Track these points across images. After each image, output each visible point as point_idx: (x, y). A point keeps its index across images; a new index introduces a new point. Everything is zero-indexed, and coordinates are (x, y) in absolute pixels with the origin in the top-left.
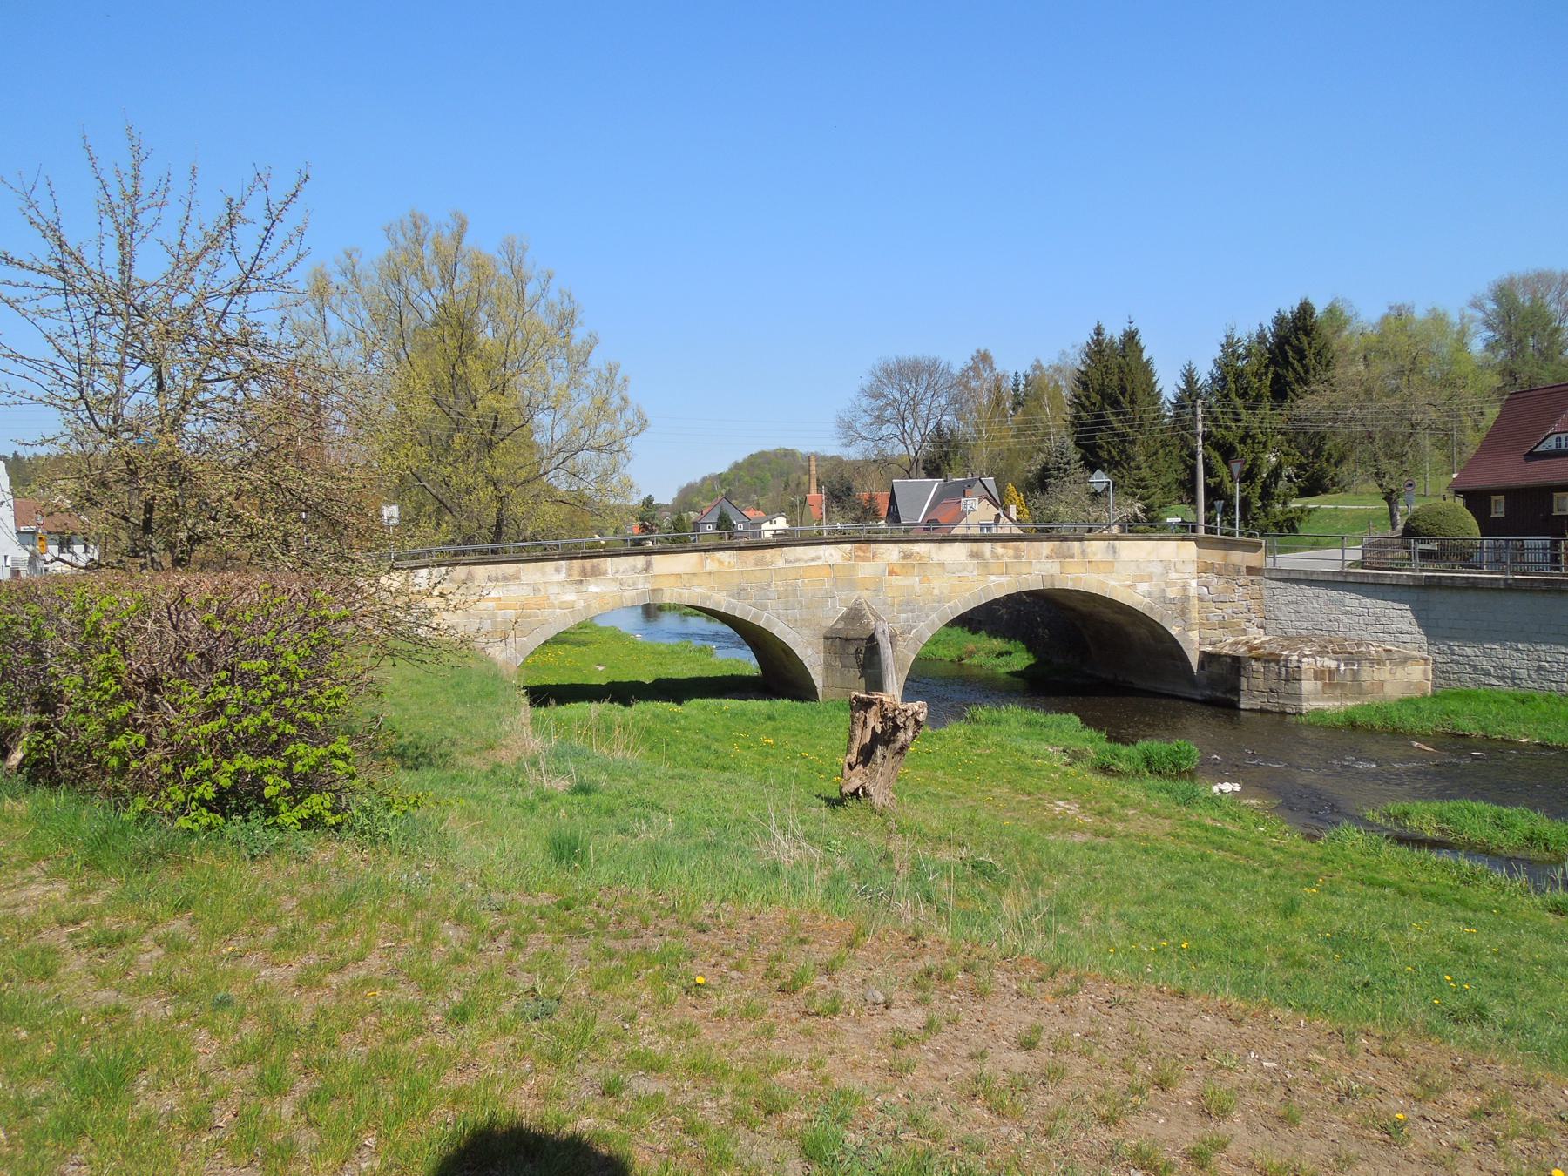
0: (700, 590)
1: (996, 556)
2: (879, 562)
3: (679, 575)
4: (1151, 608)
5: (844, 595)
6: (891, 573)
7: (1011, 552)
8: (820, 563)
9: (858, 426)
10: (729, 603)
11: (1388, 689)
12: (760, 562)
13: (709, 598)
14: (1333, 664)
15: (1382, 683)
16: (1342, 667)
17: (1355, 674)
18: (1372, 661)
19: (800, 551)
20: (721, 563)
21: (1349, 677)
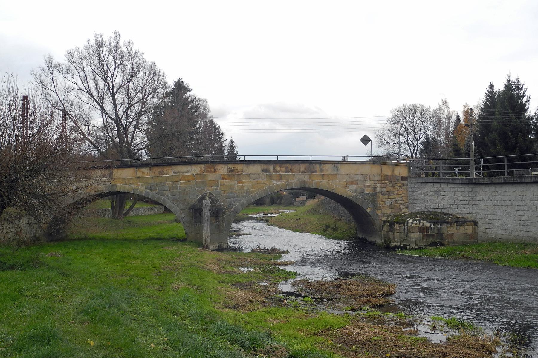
0: (133, 186)
1: (276, 171)
2: (217, 173)
3: (124, 179)
4: (357, 198)
5: (200, 189)
6: (223, 179)
7: (284, 169)
8: (189, 174)
9: (385, 137)
10: (146, 192)
11: (455, 237)
12: (161, 173)
13: (137, 189)
14: (428, 224)
15: (453, 234)
16: (433, 226)
17: (439, 229)
18: (448, 223)
19: (180, 168)
20: (143, 173)
21: (436, 231)
